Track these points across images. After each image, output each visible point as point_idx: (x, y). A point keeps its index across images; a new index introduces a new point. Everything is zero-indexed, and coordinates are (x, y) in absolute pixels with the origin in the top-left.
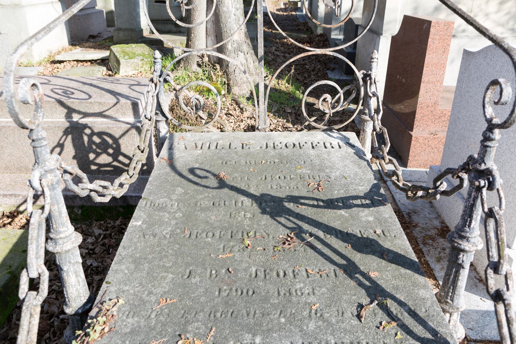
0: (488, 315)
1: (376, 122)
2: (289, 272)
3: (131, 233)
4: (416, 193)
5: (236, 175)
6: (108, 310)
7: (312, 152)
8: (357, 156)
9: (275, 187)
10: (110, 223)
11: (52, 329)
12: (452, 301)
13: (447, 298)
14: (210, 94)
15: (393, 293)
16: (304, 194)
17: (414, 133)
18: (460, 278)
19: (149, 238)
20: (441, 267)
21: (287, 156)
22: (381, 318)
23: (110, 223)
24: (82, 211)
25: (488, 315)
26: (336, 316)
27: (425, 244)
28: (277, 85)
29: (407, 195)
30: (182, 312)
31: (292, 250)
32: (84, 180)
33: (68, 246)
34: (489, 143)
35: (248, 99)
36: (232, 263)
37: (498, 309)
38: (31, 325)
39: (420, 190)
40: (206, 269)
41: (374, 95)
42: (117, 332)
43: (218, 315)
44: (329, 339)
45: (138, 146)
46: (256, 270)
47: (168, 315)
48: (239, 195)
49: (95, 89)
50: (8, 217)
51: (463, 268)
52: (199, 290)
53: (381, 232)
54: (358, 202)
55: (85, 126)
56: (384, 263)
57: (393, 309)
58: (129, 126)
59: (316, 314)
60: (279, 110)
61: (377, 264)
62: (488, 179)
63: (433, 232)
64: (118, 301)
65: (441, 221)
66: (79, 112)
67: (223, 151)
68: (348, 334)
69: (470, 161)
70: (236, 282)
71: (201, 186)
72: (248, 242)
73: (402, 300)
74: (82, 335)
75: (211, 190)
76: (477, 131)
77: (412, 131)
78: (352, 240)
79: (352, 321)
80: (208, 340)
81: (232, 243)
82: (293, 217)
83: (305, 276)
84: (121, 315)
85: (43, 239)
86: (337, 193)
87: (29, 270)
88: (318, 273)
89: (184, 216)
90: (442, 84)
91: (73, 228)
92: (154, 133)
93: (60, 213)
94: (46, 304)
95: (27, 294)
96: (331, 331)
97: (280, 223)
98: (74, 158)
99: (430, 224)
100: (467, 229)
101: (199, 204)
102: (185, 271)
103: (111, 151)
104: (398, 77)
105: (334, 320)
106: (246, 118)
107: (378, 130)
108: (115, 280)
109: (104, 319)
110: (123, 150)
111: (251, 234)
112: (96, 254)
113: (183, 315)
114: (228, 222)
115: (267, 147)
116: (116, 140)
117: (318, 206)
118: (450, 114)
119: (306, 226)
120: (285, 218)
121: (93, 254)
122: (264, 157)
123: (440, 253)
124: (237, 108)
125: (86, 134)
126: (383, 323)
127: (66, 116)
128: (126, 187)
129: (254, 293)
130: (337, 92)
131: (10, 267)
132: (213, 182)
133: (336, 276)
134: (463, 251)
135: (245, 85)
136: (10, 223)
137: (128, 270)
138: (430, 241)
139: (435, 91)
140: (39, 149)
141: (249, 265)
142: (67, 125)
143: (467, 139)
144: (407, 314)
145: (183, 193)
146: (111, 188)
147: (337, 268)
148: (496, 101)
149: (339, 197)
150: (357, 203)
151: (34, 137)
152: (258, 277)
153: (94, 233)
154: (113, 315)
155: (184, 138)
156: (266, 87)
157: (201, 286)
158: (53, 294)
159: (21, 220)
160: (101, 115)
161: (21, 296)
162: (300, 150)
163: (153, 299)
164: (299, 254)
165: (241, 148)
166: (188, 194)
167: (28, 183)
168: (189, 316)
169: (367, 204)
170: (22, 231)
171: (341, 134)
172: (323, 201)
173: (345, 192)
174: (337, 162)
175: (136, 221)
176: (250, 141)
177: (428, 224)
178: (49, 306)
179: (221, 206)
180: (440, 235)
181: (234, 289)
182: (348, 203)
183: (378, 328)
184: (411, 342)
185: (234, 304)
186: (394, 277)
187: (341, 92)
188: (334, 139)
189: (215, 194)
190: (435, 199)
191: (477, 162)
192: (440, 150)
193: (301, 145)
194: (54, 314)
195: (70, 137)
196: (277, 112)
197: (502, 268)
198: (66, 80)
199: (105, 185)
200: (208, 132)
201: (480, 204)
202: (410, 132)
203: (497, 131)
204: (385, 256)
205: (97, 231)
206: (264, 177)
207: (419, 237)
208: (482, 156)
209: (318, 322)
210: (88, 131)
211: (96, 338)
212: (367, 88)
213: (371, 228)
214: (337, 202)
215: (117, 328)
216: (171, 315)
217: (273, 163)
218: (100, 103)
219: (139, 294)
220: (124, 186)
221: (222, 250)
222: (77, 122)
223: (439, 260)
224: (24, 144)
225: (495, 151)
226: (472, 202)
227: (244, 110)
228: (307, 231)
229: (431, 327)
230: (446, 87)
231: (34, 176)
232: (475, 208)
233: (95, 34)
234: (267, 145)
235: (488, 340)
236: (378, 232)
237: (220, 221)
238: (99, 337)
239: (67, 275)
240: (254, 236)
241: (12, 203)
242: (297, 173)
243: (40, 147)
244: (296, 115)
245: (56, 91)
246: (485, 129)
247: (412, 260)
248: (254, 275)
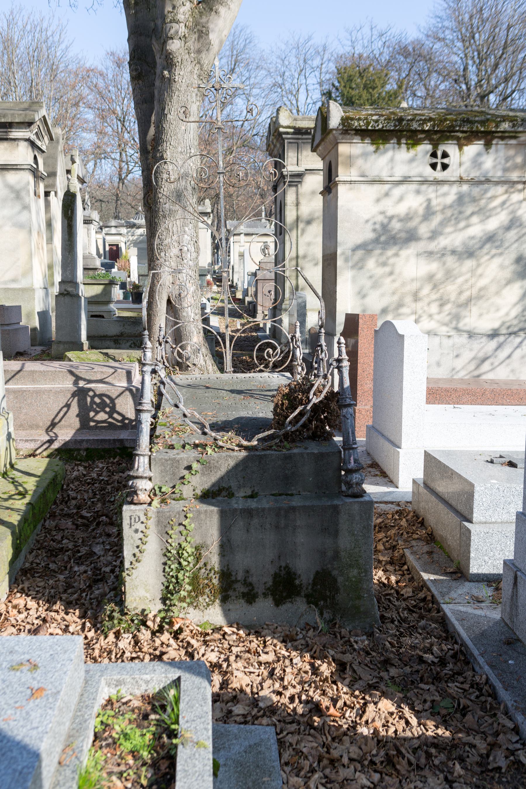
55: (90, 390)
66: (85, 380)
98: (77, 416)
103: (107, 409)
116: (112, 400)
160: (101, 381)
195: (76, 398)
210: (91, 393)
218: (102, 372)
233: (22, 351)
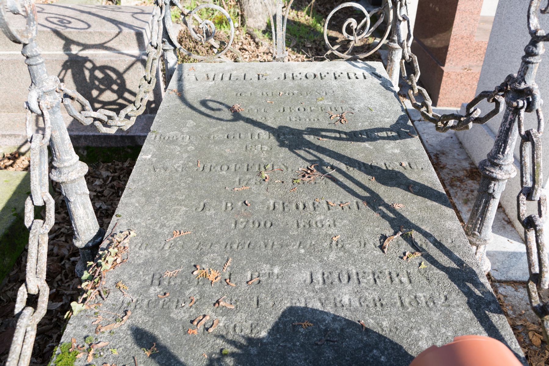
0: (515, 256)
1: (406, 49)
2: (309, 205)
3: (140, 166)
4: (447, 122)
5: (251, 107)
6: (119, 243)
7: (334, 83)
8: (384, 86)
9: (294, 119)
10: (118, 165)
11: (64, 271)
12: (480, 233)
13: (474, 230)
14: (222, 27)
15: (419, 224)
16: (325, 126)
17: (445, 69)
18: (490, 209)
19: (160, 171)
20: (468, 209)
21: (307, 88)
22: (405, 249)
23: (118, 165)
24: (88, 152)
25: (515, 256)
26: (357, 247)
27: (452, 186)
28: (296, 18)
29: (437, 125)
30: (197, 244)
31: (313, 182)
32: (87, 108)
33: (73, 176)
34: (531, 59)
35: (264, 32)
36: (249, 196)
37: (528, 236)
38: (39, 254)
39: (452, 119)
40: (221, 202)
41: (405, 18)
42: (130, 263)
43: (235, 246)
44: (350, 269)
45: (145, 77)
46: (274, 203)
47: (183, 246)
48: (256, 128)
49: (95, 18)
50: (9, 159)
51: (494, 198)
52: (214, 222)
53: (408, 164)
54: (384, 134)
55: (86, 59)
56: (409, 195)
57: (417, 240)
58: (134, 59)
59: (337, 245)
60: (299, 45)
61: (403, 196)
62: (528, 100)
63: (461, 174)
64: (130, 234)
65: (471, 162)
66: (78, 44)
67: (237, 82)
68: (370, 264)
69: (509, 81)
70: (253, 214)
71: (214, 118)
72: (266, 175)
73: (428, 231)
74: (93, 266)
75: (225, 123)
76: (516, 62)
77: (444, 65)
78: (376, 172)
79: (375, 252)
80: (224, 271)
81: (248, 176)
82: (314, 150)
83: (326, 208)
84: (133, 247)
85: (46, 166)
86: (361, 126)
87: (33, 197)
88: (340, 205)
89: (196, 149)
90: (479, 12)
91: (77, 157)
92: (161, 67)
93: (63, 140)
94: (56, 247)
95: (33, 222)
96: (352, 261)
97: (299, 156)
99: (459, 165)
100: (501, 156)
101: (212, 137)
102: (199, 204)
103: (115, 87)
104: (431, 5)
105: (355, 251)
106: (262, 54)
107: (407, 57)
108: (126, 213)
109: (116, 250)
110: (129, 86)
111: (269, 167)
112: (105, 196)
113: (198, 246)
114: (244, 155)
115: (285, 78)
116: (120, 75)
117: (340, 139)
118: (486, 46)
119: (327, 159)
120: (305, 150)
121: (102, 197)
122: (282, 88)
123: (468, 194)
124: (252, 43)
125: (87, 69)
126: (407, 254)
127: (64, 48)
128: (133, 120)
129: (272, 225)
130: (364, 16)
131: (15, 209)
132: (228, 115)
133: (358, 208)
134: (495, 179)
135: (260, 17)
136: (11, 165)
137: (139, 203)
138: (458, 183)
139: (472, 21)
140: (35, 67)
141: (265, 198)
142: (66, 58)
143: (504, 72)
144: (432, 245)
145: (195, 126)
146: (117, 118)
147: (360, 201)
148: (543, 9)
149: (363, 129)
150: (382, 136)
151: (29, 54)
152: (276, 209)
153: (102, 176)
154: (124, 247)
155: (194, 68)
156: (283, 17)
157: (216, 219)
158: (62, 237)
159: (22, 162)
160: (102, 46)
161: (27, 224)
162: (321, 81)
163: (166, 231)
164: (319, 186)
165: (257, 79)
166: (200, 126)
167: (25, 106)
168: (204, 248)
169: (393, 136)
170: (25, 172)
171: (366, 64)
172: (345, 133)
173: (369, 124)
174: (361, 93)
175: (146, 154)
176: (267, 72)
177: (457, 166)
178: (59, 249)
179: (236, 139)
180: (468, 177)
181: (251, 221)
182: (373, 135)
183: (402, 258)
184: (435, 271)
185: (252, 236)
186: (420, 209)
187: (368, 16)
188: (359, 69)
189: (229, 126)
190: (467, 127)
191: (516, 81)
192: (474, 86)
193: (323, 76)
194: (64, 256)
195: (69, 71)
196: (296, 47)
197: (536, 193)
198: (62, 8)
199: (110, 115)
200: (221, 62)
201: (517, 125)
202: (442, 67)
203: (541, 44)
204: (410, 188)
205: (105, 174)
206: (282, 109)
207: (446, 178)
208: (522, 74)
209: (339, 252)
210: (89, 65)
211: (108, 268)
212: (396, 11)
213: (397, 161)
214: (361, 134)
215: (130, 259)
216: (185, 246)
217: (291, 94)
218: (101, 33)
219: (151, 227)
220: (131, 119)
221: (237, 183)
222: (76, 55)
223: (466, 202)
224: (20, 80)
225: (537, 68)
226: (508, 126)
227: (260, 44)
228: (328, 163)
229: (457, 257)
230: (483, 17)
231: (31, 97)
232: (511, 132)
234: (285, 76)
235: (512, 281)
236: (404, 165)
237: (235, 154)
238: (111, 268)
239: (74, 207)
240: (271, 169)
241: (13, 144)
242: (318, 105)
243: (36, 65)
244: (317, 50)
245: (51, 20)
246: (528, 43)
247: (439, 192)
248: (272, 208)
